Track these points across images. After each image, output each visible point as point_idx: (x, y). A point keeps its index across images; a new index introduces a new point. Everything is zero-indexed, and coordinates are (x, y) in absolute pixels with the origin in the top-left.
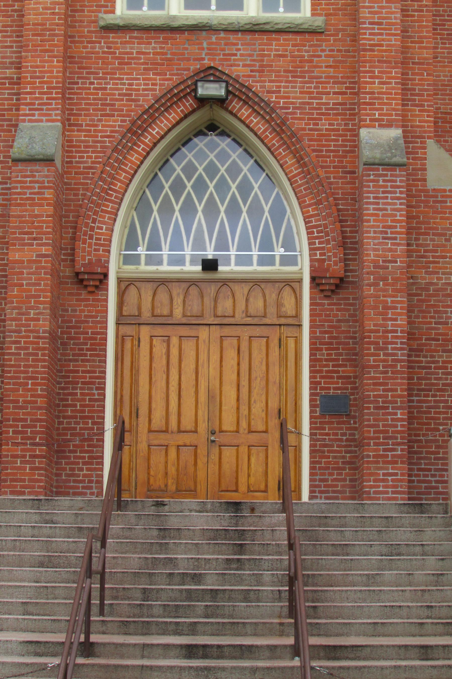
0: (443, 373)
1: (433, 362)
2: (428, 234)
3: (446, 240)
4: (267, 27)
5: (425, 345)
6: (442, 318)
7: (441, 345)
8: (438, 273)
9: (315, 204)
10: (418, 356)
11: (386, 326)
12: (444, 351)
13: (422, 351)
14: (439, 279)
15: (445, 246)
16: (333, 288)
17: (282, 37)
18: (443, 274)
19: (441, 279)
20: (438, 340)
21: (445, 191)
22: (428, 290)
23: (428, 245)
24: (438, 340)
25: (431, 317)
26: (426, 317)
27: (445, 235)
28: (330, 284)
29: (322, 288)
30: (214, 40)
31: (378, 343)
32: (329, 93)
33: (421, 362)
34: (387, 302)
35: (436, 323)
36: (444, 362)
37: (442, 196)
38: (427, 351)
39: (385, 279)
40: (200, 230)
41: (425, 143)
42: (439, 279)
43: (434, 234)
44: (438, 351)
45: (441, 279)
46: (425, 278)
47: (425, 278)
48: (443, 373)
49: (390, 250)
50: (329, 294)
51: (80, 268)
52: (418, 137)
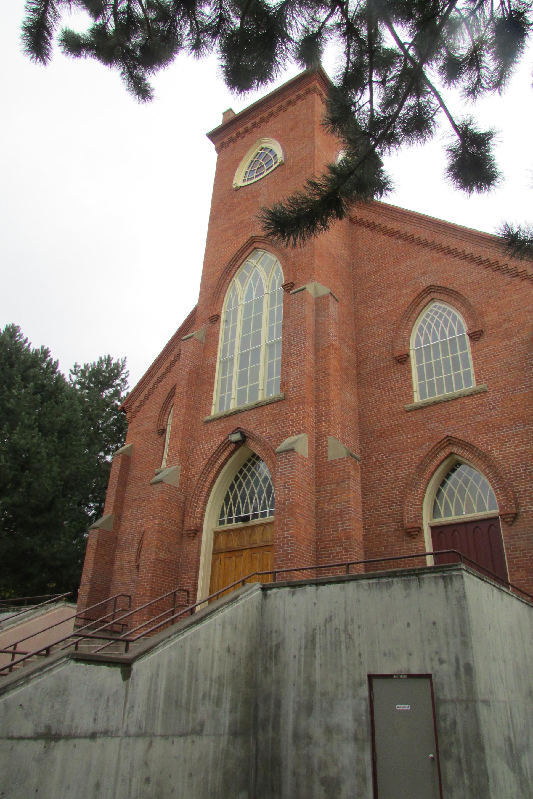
0: (337, 559)
1: (332, 553)
2: (329, 484)
3: (337, 486)
4: (262, 404)
5: (328, 544)
6: (336, 528)
7: (335, 543)
8: (333, 504)
9: (422, 477)
10: (324, 551)
11: (283, 535)
12: (337, 547)
13: (326, 548)
14: (334, 507)
15: (336, 489)
16: (512, 519)
17: (269, 406)
18: (336, 504)
19: (335, 507)
20: (334, 540)
21: (336, 460)
22: (329, 514)
23: (329, 490)
24: (334, 540)
25: (331, 529)
26: (328, 529)
27: (337, 483)
28: (510, 518)
29: (506, 520)
30: (243, 416)
31: (280, 545)
32: (286, 426)
33: (326, 554)
34: (284, 522)
35: (333, 531)
36: (337, 553)
37: (335, 463)
38: (329, 547)
39: (284, 510)
40: (457, 500)
41: (327, 438)
42: (334, 507)
43: (331, 484)
44: (334, 547)
45: (335, 507)
46: (326, 508)
47: (326, 508)
48: (337, 559)
49: (287, 494)
50: (511, 523)
51: (407, 525)
52: (324, 436)
